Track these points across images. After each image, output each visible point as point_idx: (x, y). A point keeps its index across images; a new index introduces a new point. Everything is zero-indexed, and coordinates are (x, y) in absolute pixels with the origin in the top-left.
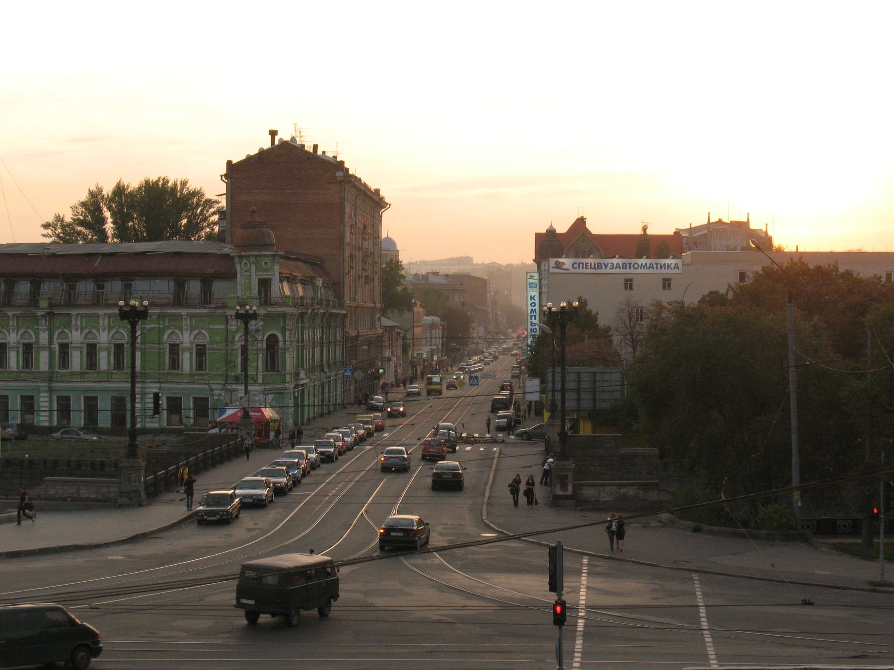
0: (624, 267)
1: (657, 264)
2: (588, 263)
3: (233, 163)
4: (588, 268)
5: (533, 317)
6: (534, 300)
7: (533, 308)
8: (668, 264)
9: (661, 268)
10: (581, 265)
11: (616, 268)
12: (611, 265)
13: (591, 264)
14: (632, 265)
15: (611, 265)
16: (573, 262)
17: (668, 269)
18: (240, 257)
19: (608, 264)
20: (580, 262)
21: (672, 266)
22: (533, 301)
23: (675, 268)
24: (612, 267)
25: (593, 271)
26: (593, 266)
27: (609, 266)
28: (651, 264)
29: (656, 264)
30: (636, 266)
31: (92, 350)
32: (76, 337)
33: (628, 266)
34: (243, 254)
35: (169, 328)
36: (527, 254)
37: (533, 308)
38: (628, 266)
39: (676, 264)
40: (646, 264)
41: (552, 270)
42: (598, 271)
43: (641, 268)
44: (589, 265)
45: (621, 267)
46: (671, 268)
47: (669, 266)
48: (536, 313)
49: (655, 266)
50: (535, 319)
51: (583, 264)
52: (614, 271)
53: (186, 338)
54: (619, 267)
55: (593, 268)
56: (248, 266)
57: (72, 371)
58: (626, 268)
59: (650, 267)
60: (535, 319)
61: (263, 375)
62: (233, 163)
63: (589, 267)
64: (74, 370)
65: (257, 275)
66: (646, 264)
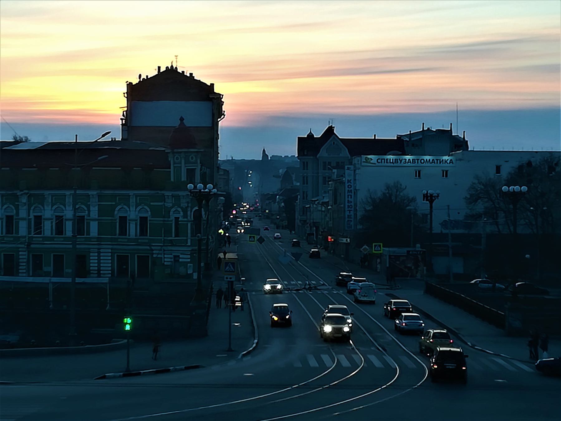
0: (396, 162)
1: (437, 160)
2: (388, 159)
3: (134, 84)
4: (388, 163)
5: (350, 197)
6: (351, 183)
7: (350, 189)
8: (445, 160)
9: (440, 163)
10: (383, 160)
11: (408, 162)
12: (405, 160)
13: (390, 159)
14: (419, 161)
15: (405, 160)
16: (377, 158)
17: (445, 163)
18: (173, 153)
19: (402, 160)
20: (383, 158)
21: (448, 162)
22: (349, 184)
23: (450, 163)
24: (405, 162)
25: (392, 164)
26: (391, 161)
27: (403, 161)
28: (433, 160)
29: (436, 160)
30: (422, 161)
31: (60, 222)
32: (48, 212)
33: (416, 161)
34: (175, 150)
35: (6, 204)
36: (293, 150)
37: (350, 189)
38: (416, 161)
39: (451, 160)
40: (429, 160)
41: (363, 164)
42: (395, 164)
43: (426, 163)
44: (389, 160)
45: (412, 162)
46: (447, 163)
47: (446, 162)
48: (352, 193)
49: (436, 161)
50: (351, 198)
51: (384, 159)
52: (406, 165)
53: (133, 214)
54: (410, 162)
55: (391, 163)
56: (179, 159)
57: (43, 236)
58: (415, 163)
59: (432, 162)
60: (351, 198)
61: (191, 240)
62: (134, 84)
63: (389, 162)
64: (45, 235)
65: (185, 166)
66: (429, 160)
